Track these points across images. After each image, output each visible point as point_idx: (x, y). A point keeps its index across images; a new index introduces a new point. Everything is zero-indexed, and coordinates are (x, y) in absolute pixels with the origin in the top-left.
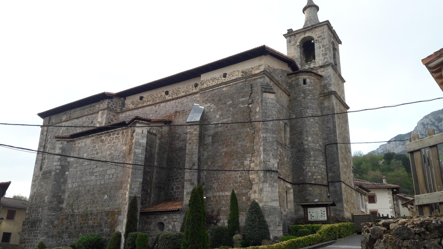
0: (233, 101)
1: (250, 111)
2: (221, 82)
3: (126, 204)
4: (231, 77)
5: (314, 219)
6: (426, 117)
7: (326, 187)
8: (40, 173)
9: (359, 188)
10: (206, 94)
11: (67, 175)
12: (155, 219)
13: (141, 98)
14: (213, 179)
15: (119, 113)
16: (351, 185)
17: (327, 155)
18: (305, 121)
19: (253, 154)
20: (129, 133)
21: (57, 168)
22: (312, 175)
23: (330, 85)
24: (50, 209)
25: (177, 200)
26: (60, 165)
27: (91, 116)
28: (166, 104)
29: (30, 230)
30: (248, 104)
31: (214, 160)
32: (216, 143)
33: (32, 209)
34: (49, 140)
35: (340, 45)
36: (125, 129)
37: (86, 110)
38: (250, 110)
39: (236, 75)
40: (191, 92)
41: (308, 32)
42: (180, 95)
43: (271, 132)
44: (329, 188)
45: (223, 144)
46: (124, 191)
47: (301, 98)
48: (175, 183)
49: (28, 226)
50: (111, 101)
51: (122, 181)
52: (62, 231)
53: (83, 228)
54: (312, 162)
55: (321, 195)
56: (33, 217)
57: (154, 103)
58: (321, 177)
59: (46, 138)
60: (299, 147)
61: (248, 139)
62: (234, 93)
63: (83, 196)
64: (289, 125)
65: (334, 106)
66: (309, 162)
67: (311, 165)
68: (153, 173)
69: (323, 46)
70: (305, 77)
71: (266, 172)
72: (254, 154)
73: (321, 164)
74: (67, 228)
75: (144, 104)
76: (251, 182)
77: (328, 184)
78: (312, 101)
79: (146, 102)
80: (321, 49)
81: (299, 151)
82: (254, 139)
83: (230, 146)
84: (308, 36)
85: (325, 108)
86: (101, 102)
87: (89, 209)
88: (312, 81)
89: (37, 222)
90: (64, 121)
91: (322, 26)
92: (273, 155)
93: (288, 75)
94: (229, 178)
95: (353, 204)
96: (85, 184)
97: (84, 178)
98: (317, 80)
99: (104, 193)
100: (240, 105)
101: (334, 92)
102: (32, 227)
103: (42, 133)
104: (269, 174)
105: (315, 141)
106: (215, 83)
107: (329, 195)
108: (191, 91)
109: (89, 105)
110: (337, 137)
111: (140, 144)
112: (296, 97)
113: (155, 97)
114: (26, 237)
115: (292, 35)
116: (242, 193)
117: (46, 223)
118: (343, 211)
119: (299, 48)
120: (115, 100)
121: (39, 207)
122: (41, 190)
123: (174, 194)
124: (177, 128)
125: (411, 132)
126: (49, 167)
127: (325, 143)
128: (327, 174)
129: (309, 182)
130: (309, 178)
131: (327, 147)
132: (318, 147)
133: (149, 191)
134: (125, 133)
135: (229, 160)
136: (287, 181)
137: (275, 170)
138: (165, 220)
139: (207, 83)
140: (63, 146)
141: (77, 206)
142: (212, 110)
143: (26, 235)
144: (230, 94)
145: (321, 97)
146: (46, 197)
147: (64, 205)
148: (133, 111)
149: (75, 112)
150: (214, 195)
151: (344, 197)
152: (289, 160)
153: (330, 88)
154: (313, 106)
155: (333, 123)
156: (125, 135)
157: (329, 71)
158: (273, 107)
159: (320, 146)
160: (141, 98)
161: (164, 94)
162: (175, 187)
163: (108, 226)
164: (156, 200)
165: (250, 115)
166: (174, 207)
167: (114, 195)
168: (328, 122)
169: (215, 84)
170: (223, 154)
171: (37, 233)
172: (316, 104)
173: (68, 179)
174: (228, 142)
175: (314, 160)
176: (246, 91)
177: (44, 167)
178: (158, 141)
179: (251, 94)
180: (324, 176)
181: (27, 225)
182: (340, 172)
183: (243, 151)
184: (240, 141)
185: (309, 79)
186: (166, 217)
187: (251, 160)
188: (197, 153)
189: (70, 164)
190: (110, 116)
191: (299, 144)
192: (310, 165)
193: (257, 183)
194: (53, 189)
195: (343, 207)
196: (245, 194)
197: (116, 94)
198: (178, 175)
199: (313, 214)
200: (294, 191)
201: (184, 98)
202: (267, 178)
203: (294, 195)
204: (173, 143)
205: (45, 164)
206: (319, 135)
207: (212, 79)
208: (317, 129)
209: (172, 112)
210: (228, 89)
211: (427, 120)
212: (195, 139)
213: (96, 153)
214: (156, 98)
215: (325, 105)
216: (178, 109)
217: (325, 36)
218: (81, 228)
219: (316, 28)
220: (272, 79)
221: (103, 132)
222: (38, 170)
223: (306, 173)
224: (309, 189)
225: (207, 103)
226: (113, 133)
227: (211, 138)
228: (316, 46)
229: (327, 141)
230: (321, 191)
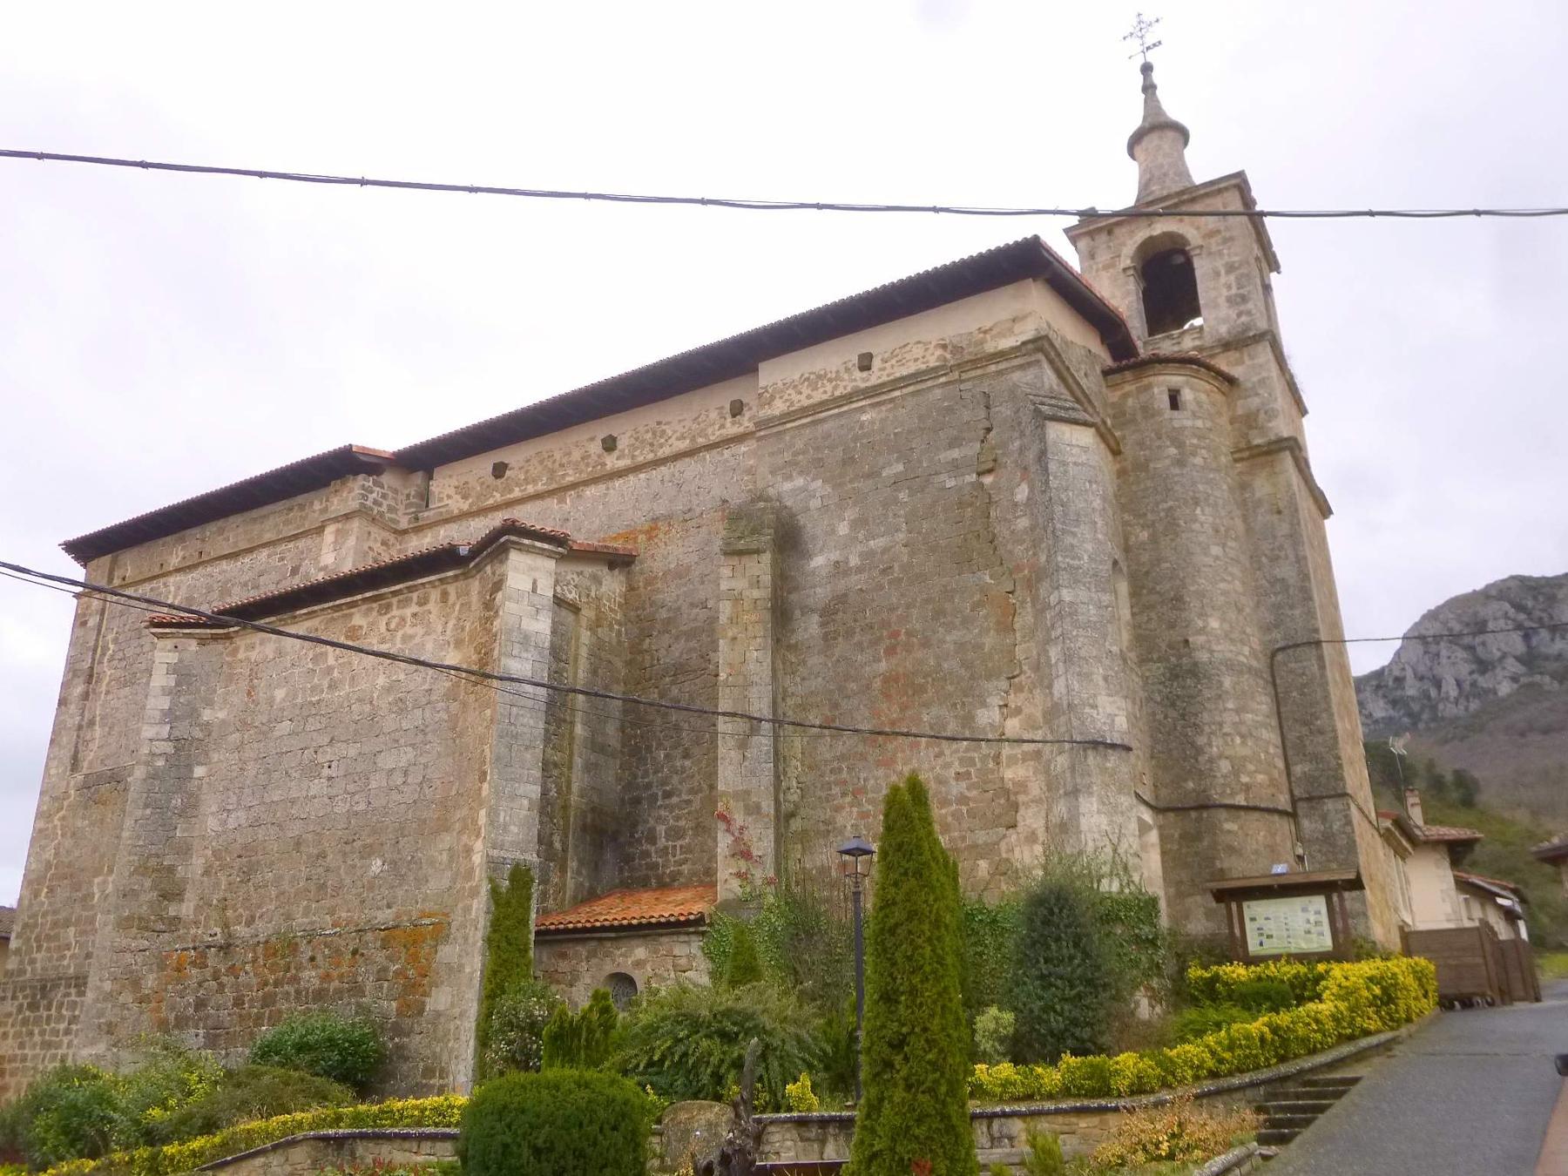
0: (908, 462)
2: (849, 389)
3: (474, 893)
4: (892, 366)
5: (1270, 947)
6: (1432, 616)
7: (1285, 819)
8: (72, 783)
10: (787, 438)
11: (199, 779)
12: (594, 961)
13: (499, 470)
14: (836, 790)
15: (405, 532)
19: (1014, 677)
20: (474, 597)
21: (158, 751)
22: (1236, 772)
24: (124, 924)
25: (676, 884)
26: (169, 739)
27: (291, 545)
28: (608, 489)
29: (25, 1022)
30: (979, 474)
32: (840, 639)
33: (37, 930)
34: (111, 646)
35: (1273, 275)
36: (456, 578)
37: (271, 522)
39: (916, 360)
40: (715, 435)
42: (665, 451)
44: (1297, 824)
45: (875, 643)
46: (459, 840)
47: (1167, 462)
48: (662, 813)
49: (16, 1003)
50: (375, 483)
51: (446, 798)
52: (176, 1018)
53: (274, 1003)
55: (1273, 851)
56: (38, 965)
57: (554, 486)
59: (97, 640)
60: (1173, 659)
61: (986, 617)
62: (910, 432)
63: (272, 863)
66: (1218, 719)
67: (1226, 729)
68: (570, 768)
69: (1230, 268)
70: (1176, 380)
71: (1085, 750)
72: (1016, 680)
73: (1265, 725)
74: (200, 1004)
75: (511, 491)
76: (1012, 798)
79: (517, 485)
80: (1223, 279)
81: (1175, 675)
83: (908, 648)
85: (1259, 503)
86: (332, 488)
87: (300, 920)
88: (1203, 397)
89: (55, 986)
90: (178, 570)
91: (1220, 191)
92: (1106, 679)
95: (1383, 889)
96: (278, 815)
97: (278, 787)
98: (1219, 397)
99: (368, 852)
100: (942, 477)
101: (1292, 443)
102: (33, 1006)
103: (80, 621)
105: (1235, 635)
106: (825, 392)
107: (1300, 851)
108: (718, 433)
109: (281, 503)
111: (525, 640)
112: (1148, 461)
113: (557, 464)
114: (10, 1052)
115: (1100, 230)
116: (975, 846)
117: (108, 986)
118: (1365, 914)
119: (1132, 278)
120: (388, 479)
121: (67, 923)
122: (77, 854)
123: (660, 860)
124: (659, 585)
125: (1383, 669)
126: (108, 757)
131: (1280, 657)
133: (558, 845)
134: (452, 597)
135: (904, 708)
138: (639, 964)
139: (786, 397)
140: (181, 661)
141: (246, 908)
142: (815, 504)
143: (10, 1041)
144: (895, 434)
145: (1236, 461)
146: (96, 880)
147: (184, 906)
148: (464, 523)
149: (221, 531)
153: (1270, 425)
154: (1217, 493)
155: (1298, 561)
156: (454, 605)
158: (1090, 482)
159: (1253, 652)
160: (499, 470)
161: (596, 448)
162: (661, 829)
163: (389, 989)
164: (587, 884)
166: (677, 910)
167: (413, 857)
168: (1274, 559)
169: (825, 397)
170: (877, 684)
171: (56, 1032)
172: (1225, 487)
173: (203, 797)
174: (895, 635)
175: (1238, 711)
176: (966, 418)
177: (89, 757)
178: (586, 637)
179: (989, 430)
180: (1276, 774)
181: (14, 998)
182: (1339, 758)
183: (967, 668)
184: (950, 627)
185: (1194, 391)
186: (640, 952)
187: (1006, 706)
188: (768, 680)
189: (214, 735)
190: (371, 544)
191: (1170, 646)
192: (1225, 730)
193: (1038, 801)
194: (138, 838)
196: (989, 850)
197: (394, 454)
198: (675, 779)
199: (1270, 927)
201: (687, 460)
202: (1089, 775)
203: (1163, 853)
204: (645, 646)
205: (94, 746)
206: (1248, 610)
207: (807, 379)
209: (640, 519)
210: (883, 415)
211: (1433, 629)
213: (326, 684)
214: (562, 465)
215: (1258, 495)
216: (661, 509)
218: (268, 1000)
220: (1065, 373)
221: (359, 597)
222: (64, 772)
224: (1228, 826)
225: (791, 476)
226: (401, 597)
227: (815, 618)
228: (1201, 267)
230: (1273, 835)
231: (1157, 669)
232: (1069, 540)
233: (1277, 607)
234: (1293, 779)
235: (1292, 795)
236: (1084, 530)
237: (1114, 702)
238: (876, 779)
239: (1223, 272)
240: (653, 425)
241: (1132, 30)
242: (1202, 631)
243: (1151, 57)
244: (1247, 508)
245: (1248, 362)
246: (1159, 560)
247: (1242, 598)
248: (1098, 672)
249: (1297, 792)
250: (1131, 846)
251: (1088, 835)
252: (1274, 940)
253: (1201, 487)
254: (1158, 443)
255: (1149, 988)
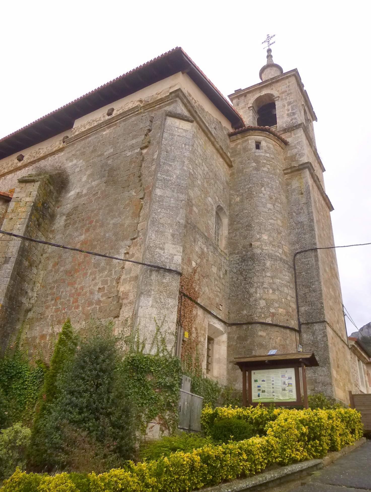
1: (143, 160)
5: (265, 398)
9: (356, 346)
14: (50, 298)
16: (342, 335)
17: (297, 272)
18: (258, 206)
19: (134, 239)
22: (268, 307)
23: (301, 155)
28: (15, 175)
31: (60, 260)
32: (70, 226)
35: (314, 122)
38: (142, 157)
41: (265, 89)
43: (174, 188)
44: (300, 336)
47: (251, 169)
54: (267, 281)
58: (284, 311)
60: (244, 253)
61: (129, 211)
64: (228, 213)
65: (309, 186)
66: (261, 280)
69: (289, 104)
70: (259, 138)
71: (151, 271)
73: (287, 286)
76: (121, 301)
77: (300, 327)
78: (271, 176)
80: (286, 108)
81: (244, 260)
82: (141, 210)
84: (265, 94)
91: (287, 77)
92: (173, 235)
93: (230, 135)
94: (79, 294)
95: (348, 373)
98: (279, 149)
100: (126, 152)
101: (309, 165)
104: (157, 276)
105: (275, 243)
110: (315, 239)
112: (243, 169)
118: (331, 384)
119: (252, 111)
127: (294, 249)
128: (298, 307)
129: (261, 321)
130: (260, 310)
131: (298, 256)
132: (280, 254)
136: (215, 314)
137: (174, 269)
144: (114, 138)
145: (285, 174)
150: (44, 333)
151: (332, 355)
152: (223, 274)
153: (301, 159)
154: (273, 183)
155: (309, 214)
157: (299, 135)
158: (185, 144)
159: (285, 253)
165: (141, 166)
168: (298, 214)
174: (91, 222)
175: (272, 277)
179: (150, 130)
182: (322, 303)
192: (264, 286)
195: (330, 375)
199: (264, 386)
200: (229, 338)
202: (151, 285)
203: (229, 346)
208: (279, 222)
210: (111, 131)
212: (23, 210)
215: (293, 187)
217: (292, 91)
219: (277, 81)
223: (256, 300)
224: (260, 333)
229: (297, 246)
230: (285, 340)
231: (236, 257)
232: (167, 167)
233: (298, 234)
234: (300, 314)
235: (299, 322)
236: (177, 164)
237: (176, 248)
238: (66, 292)
239: (286, 105)
240: (37, 150)
241: (265, 40)
242: (259, 240)
243: (271, 47)
244: (288, 193)
245: (293, 136)
246: (243, 209)
247: (281, 228)
248: (169, 232)
249: (301, 320)
250: (169, 328)
251: (142, 319)
252: (266, 393)
253: (265, 179)
254: (249, 161)
255: (162, 418)
